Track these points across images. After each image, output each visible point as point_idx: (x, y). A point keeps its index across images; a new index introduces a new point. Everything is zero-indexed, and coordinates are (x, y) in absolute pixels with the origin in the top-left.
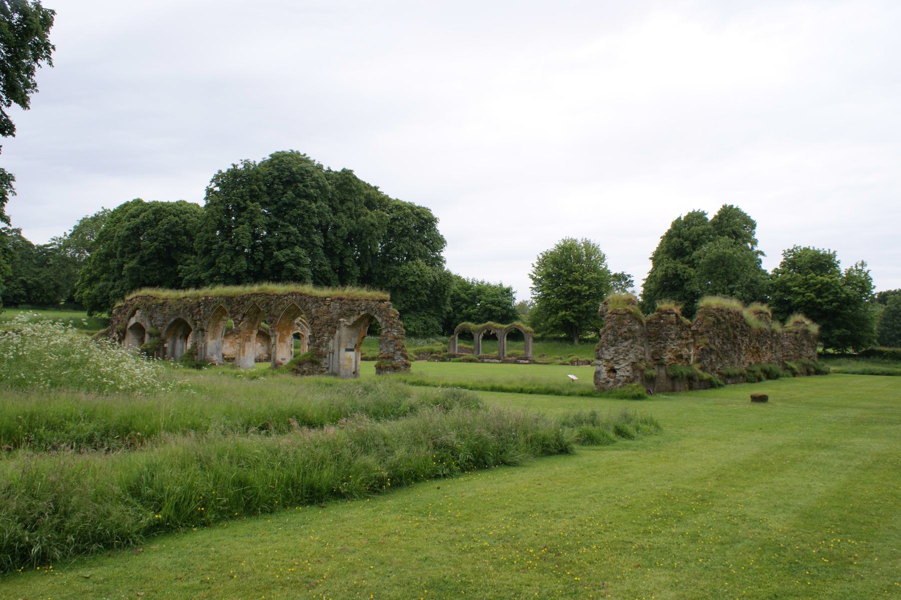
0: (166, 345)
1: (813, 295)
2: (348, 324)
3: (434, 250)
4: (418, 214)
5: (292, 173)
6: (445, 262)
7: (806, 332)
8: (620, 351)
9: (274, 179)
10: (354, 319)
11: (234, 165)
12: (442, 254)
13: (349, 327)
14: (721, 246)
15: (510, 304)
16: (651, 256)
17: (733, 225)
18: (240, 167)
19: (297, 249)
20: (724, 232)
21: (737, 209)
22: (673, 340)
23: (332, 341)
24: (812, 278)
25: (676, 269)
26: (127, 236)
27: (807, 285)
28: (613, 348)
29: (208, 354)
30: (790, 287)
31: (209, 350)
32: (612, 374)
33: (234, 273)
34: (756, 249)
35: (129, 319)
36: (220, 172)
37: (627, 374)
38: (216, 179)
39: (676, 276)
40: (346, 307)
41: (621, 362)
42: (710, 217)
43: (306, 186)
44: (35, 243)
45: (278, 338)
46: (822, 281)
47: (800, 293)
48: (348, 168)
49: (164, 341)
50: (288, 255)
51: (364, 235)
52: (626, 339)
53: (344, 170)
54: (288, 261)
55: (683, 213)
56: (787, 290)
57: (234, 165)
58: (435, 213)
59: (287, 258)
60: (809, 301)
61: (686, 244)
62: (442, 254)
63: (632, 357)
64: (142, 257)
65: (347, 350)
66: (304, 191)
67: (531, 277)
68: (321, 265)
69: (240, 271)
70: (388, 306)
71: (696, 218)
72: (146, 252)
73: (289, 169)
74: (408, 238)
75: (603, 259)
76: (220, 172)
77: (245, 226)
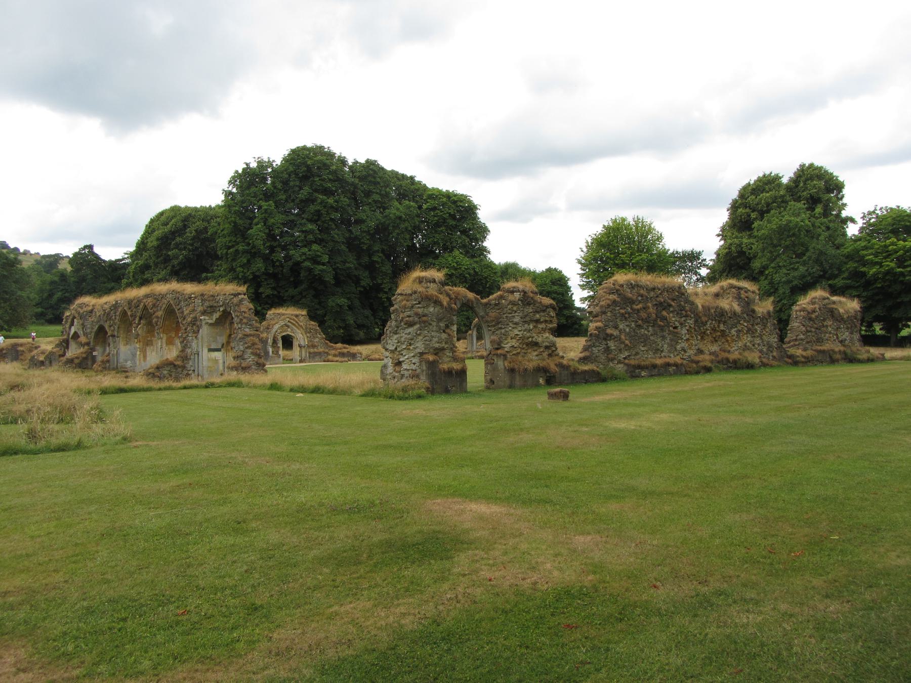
0: (94, 354)
1: (892, 265)
2: (210, 321)
3: (477, 240)
4: (455, 202)
5: (308, 166)
6: (489, 252)
7: (832, 313)
8: (403, 339)
9: (290, 175)
10: (216, 316)
11: (247, 164)
12: (485, 244)
13: (211, 325)
14: (796, 215)
15: (63, 276)
16: (718, 231)
17: (816, 189)
18: (254, 165)
19: (315, 247)
20: (800, 197)
21: (811, 165)
22: (516, 324)
23: (195, 341)
24: (893, 244)
25: (740, 245)
26: (158, 246)
27: (887, 253)
28: (396, 336)
29: (121, 360)
30: (863, 257)
31: (122, 357)
32: (397, 369)
33: (251, 277)
34: (844, 214)
35: (70, 328)
36: (237, 172)
37: (414, 367)
38: (232, 182)
39: (741, 253)
40: (207, 304)
41: (404, 353)
42: (785, 180)
43: (323, 180)
44: (103, 257)
45: (164, 340)
46: (905, 247)
47: (876, 263)
48: (373, 158)
49: (93, 350)
50: (304, 254)
51: (391, 228)
52: (411, 325)
53: (368, 161)
54: (305, 260)
55: (751, 177)
56: (863, 262)
57: (247, 164)
58: (475, 201)
59: (304, 257)
60: (888, 273)
61: (753, 215)
62: (485, 244)
63: (420, 346)
64: (173, 266)
65: (210, 350)
66: (321, 185)
67: (580, 262)
68: (344, 262)
69: (257, 274)
70: (241, 301)
71: (768, 183)
72: (175, 262)
73: (305, 163)
74: (443, 228)
75: (660, 238)
76: (237, 172)
77: (259, 226)
